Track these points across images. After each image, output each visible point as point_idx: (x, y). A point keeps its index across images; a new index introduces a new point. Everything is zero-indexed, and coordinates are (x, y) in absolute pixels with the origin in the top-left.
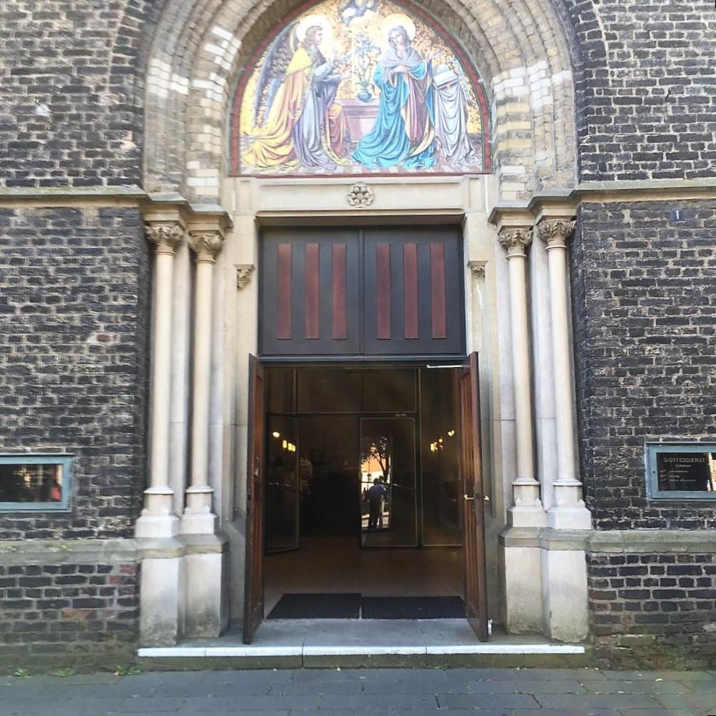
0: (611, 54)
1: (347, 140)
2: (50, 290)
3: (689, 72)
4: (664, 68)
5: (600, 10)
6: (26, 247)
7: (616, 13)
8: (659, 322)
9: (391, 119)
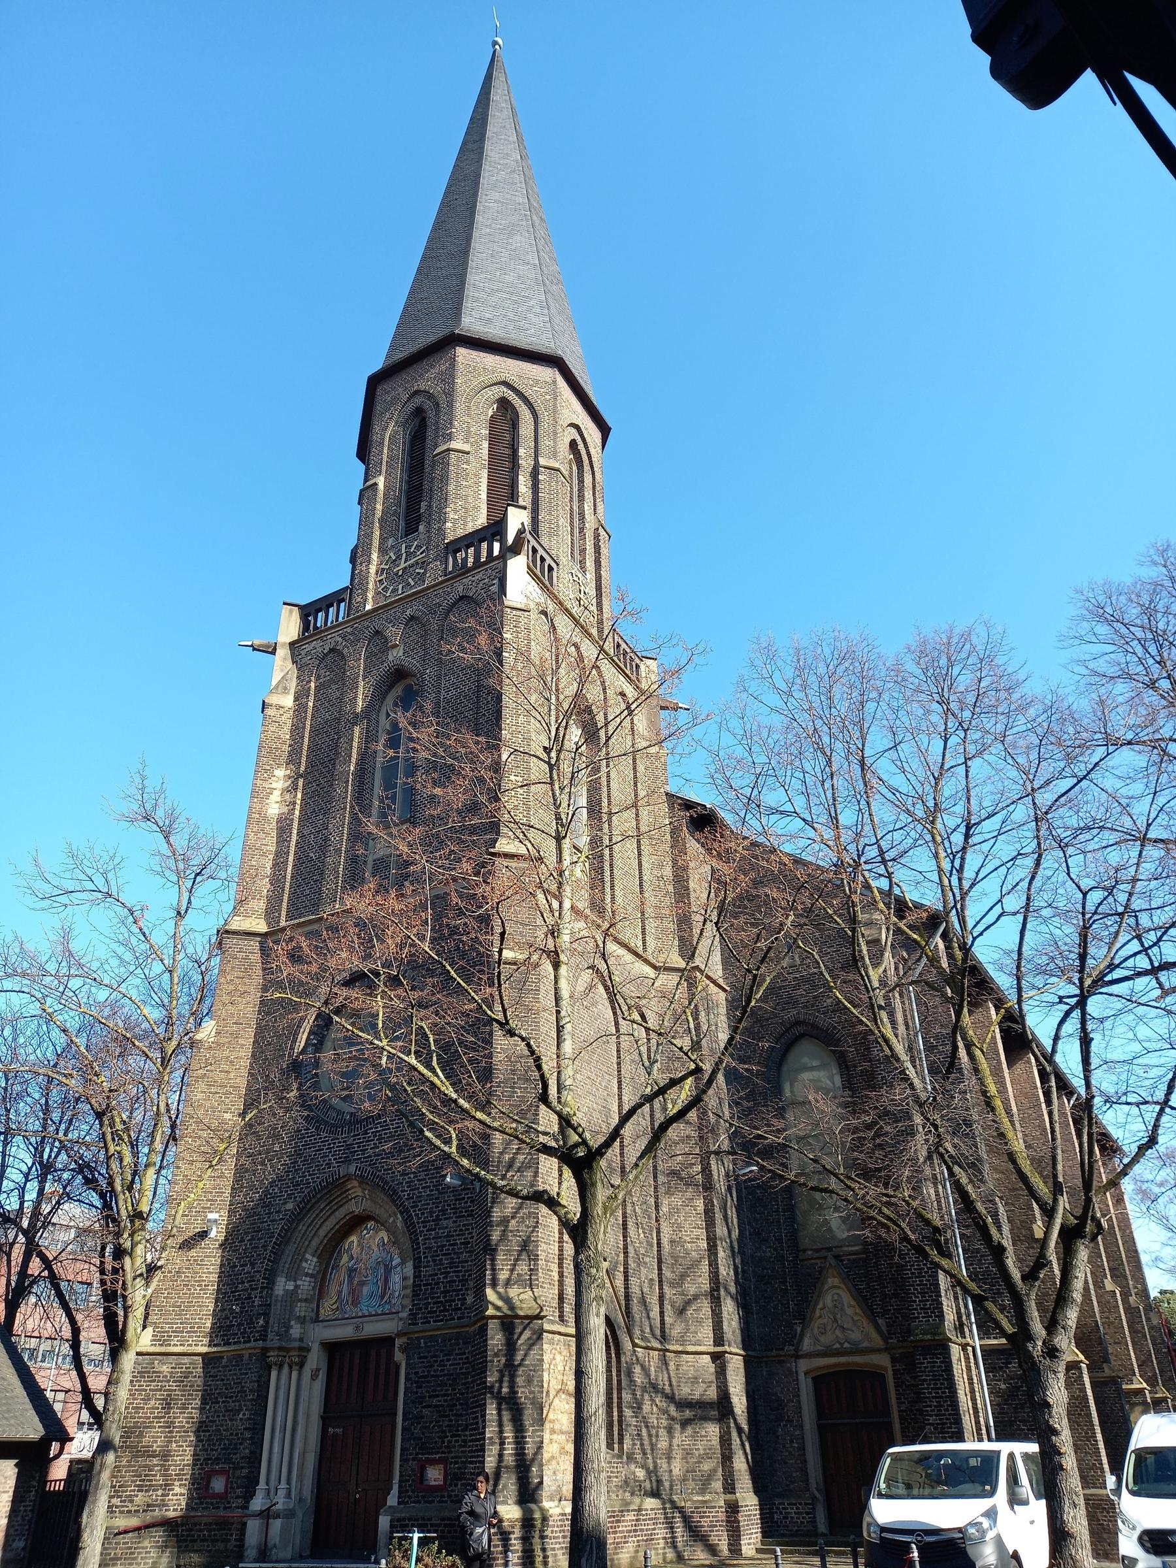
8: (429, 1397)
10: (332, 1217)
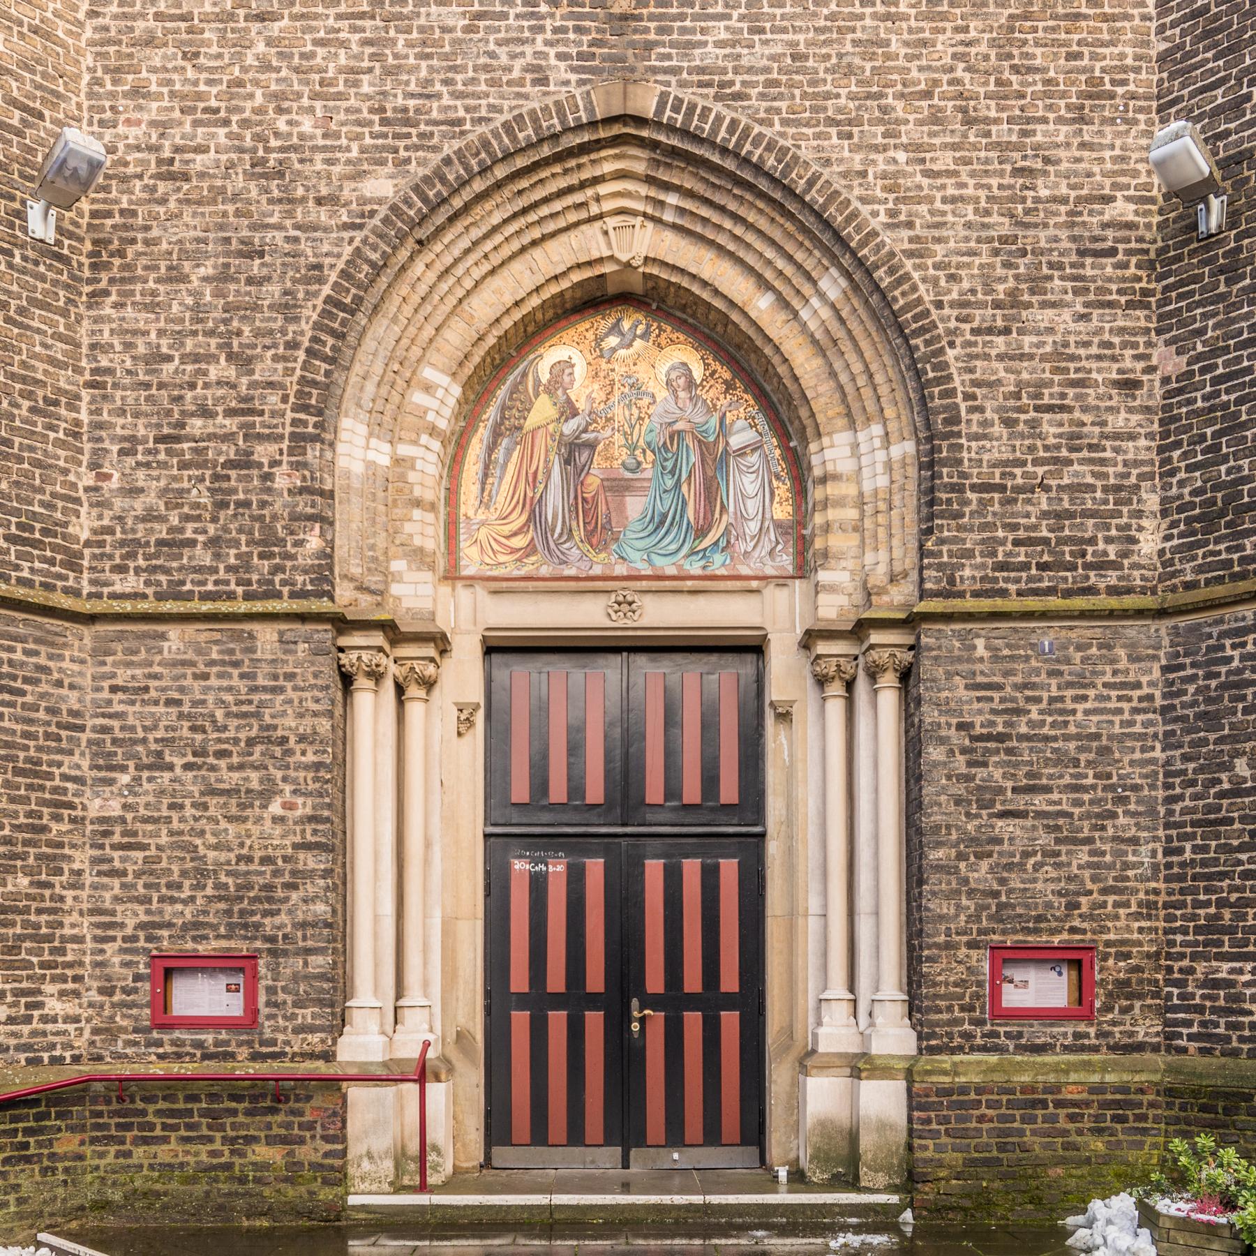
0: (969, 421)
1: (607, 527)
2: (219, 740)
3: (1072, 449)
4: (1039, 443)
5: (957, 359)
6: (185, 683)
7: (978, 363)
8: (1014, 790)
9: (668, 498)
10: (517, 266)
